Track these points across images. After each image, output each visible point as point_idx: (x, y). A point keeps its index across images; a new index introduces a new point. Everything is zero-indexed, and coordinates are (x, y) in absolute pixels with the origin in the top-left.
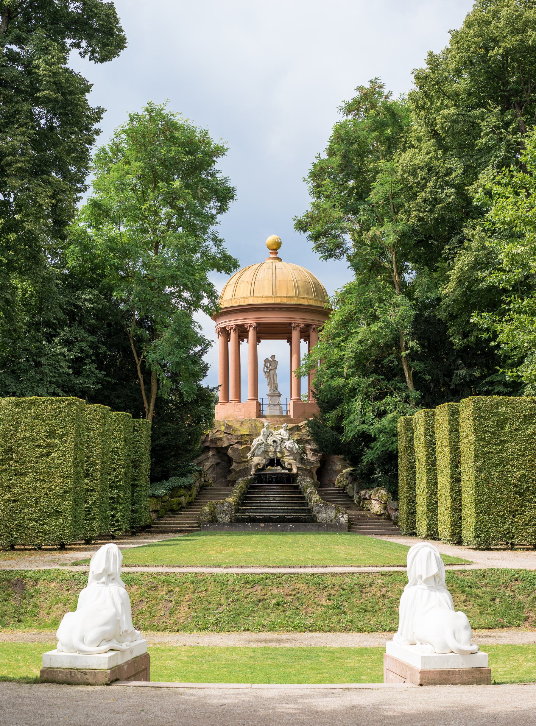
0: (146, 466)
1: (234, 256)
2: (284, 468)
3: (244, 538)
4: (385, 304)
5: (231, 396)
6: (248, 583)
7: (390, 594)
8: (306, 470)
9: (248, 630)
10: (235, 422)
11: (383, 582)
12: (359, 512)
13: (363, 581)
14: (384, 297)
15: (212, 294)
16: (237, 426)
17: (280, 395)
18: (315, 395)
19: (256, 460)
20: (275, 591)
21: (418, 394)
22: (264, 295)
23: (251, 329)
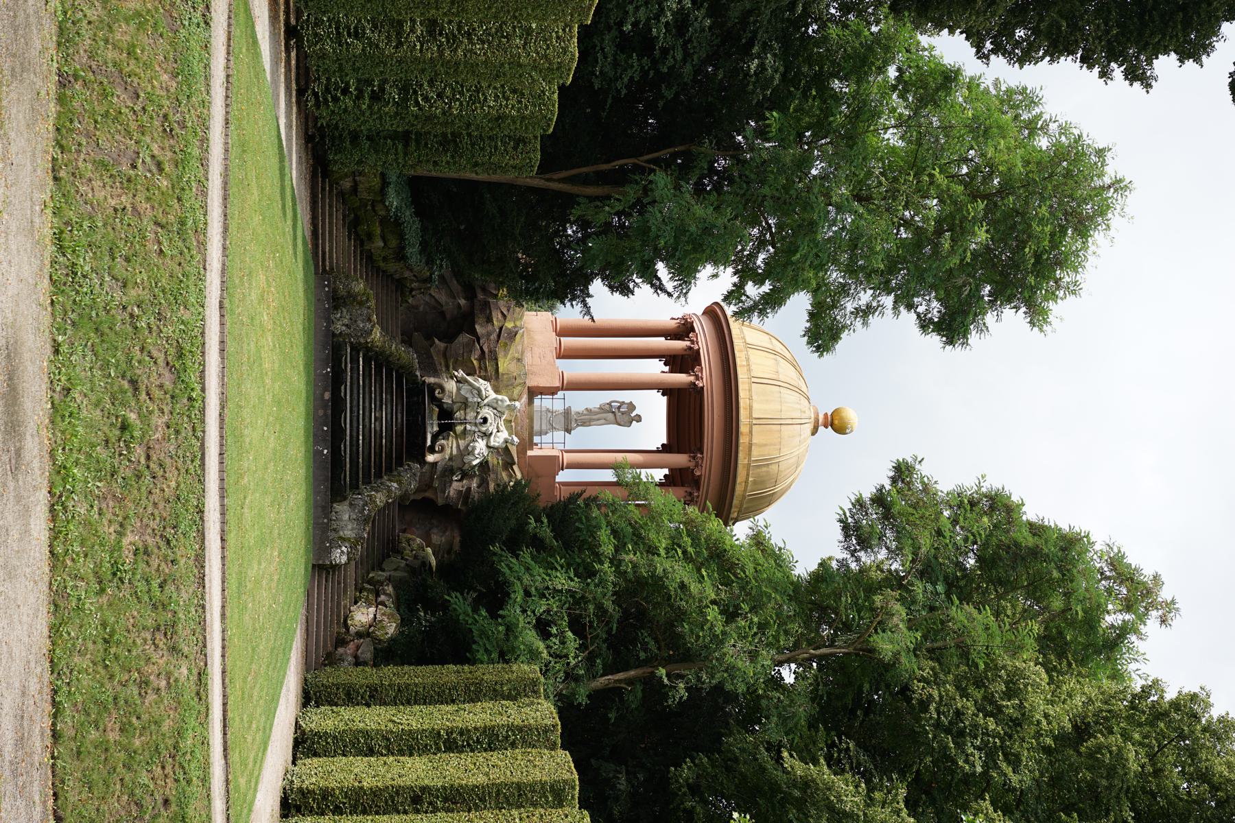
0: (447, 171)
1: (840, 346)
2: (435, 438)
4: (755, 634)
5: (567, 341)
6: (180, 355)
7: (151, 697)
8: (432, 478)
9: (56, 352)
10: (520, 348)
11: (182, 679)
12: (351, 582)
13: (183, 631)
14: (771, 632)
15: (772, 302)
16: (514, 351)
17: (568, 431)
18: (573, 498)
19: (451, 386)
20: (158, 421)
21: (582, 699)
22: (754, 401)
23: (692, 378)
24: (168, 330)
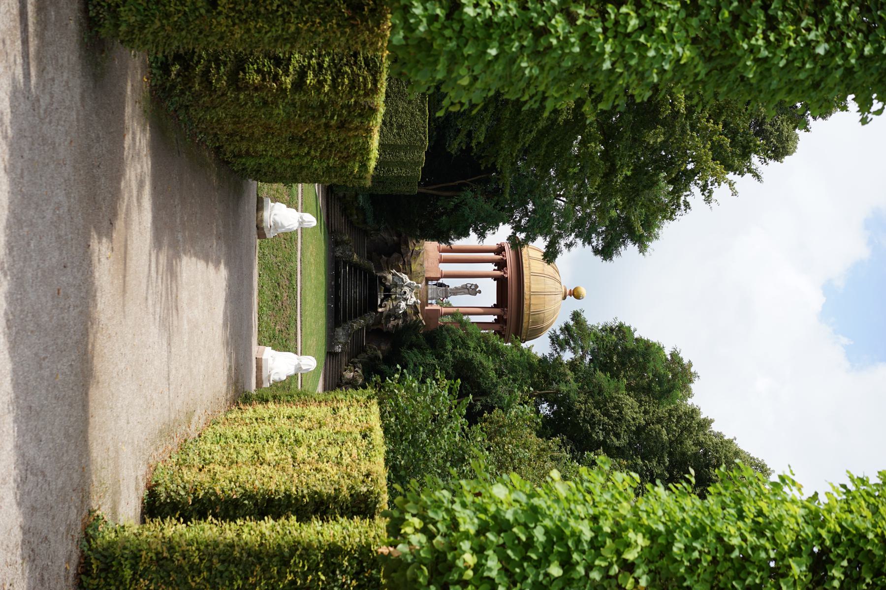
2: (382, 301)
3: (322, 269)
16: (419, 261)
19: (390, 277)
20: (285, 295)
22: (531, 284)
24: (287, 269)
